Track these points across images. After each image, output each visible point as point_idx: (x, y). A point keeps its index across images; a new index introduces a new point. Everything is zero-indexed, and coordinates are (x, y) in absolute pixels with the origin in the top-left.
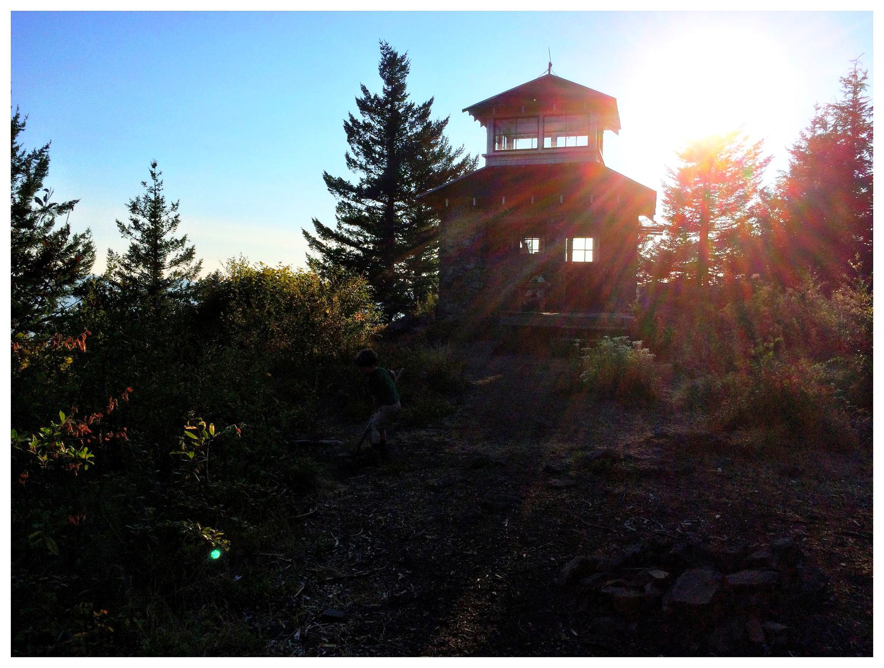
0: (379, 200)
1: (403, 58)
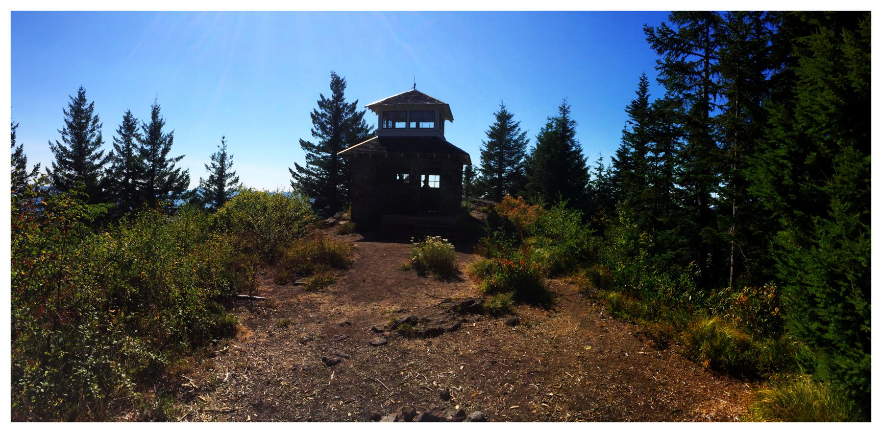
0: (329, 153)
1: (343, 80)
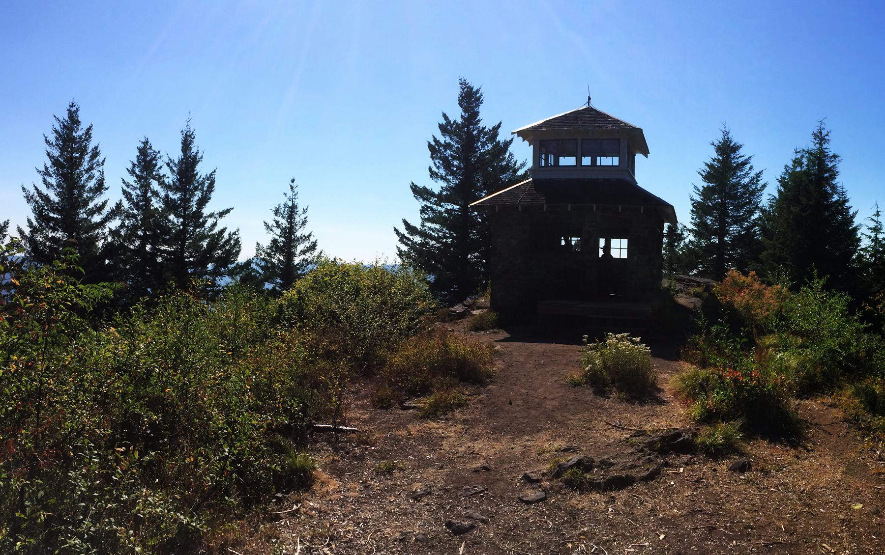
1: (478, 91)
